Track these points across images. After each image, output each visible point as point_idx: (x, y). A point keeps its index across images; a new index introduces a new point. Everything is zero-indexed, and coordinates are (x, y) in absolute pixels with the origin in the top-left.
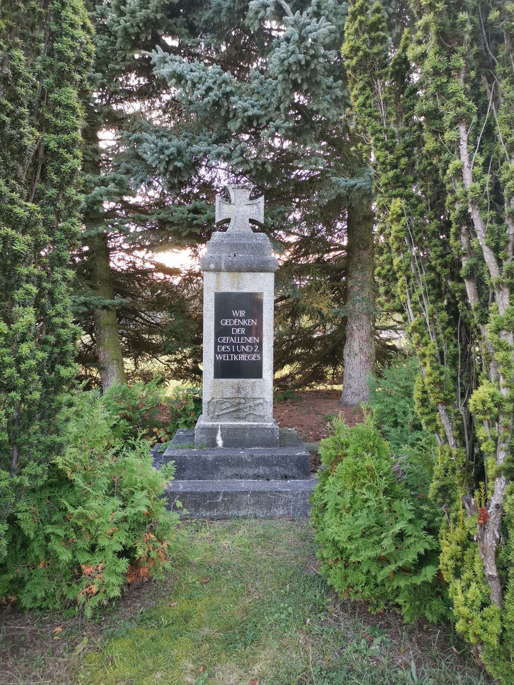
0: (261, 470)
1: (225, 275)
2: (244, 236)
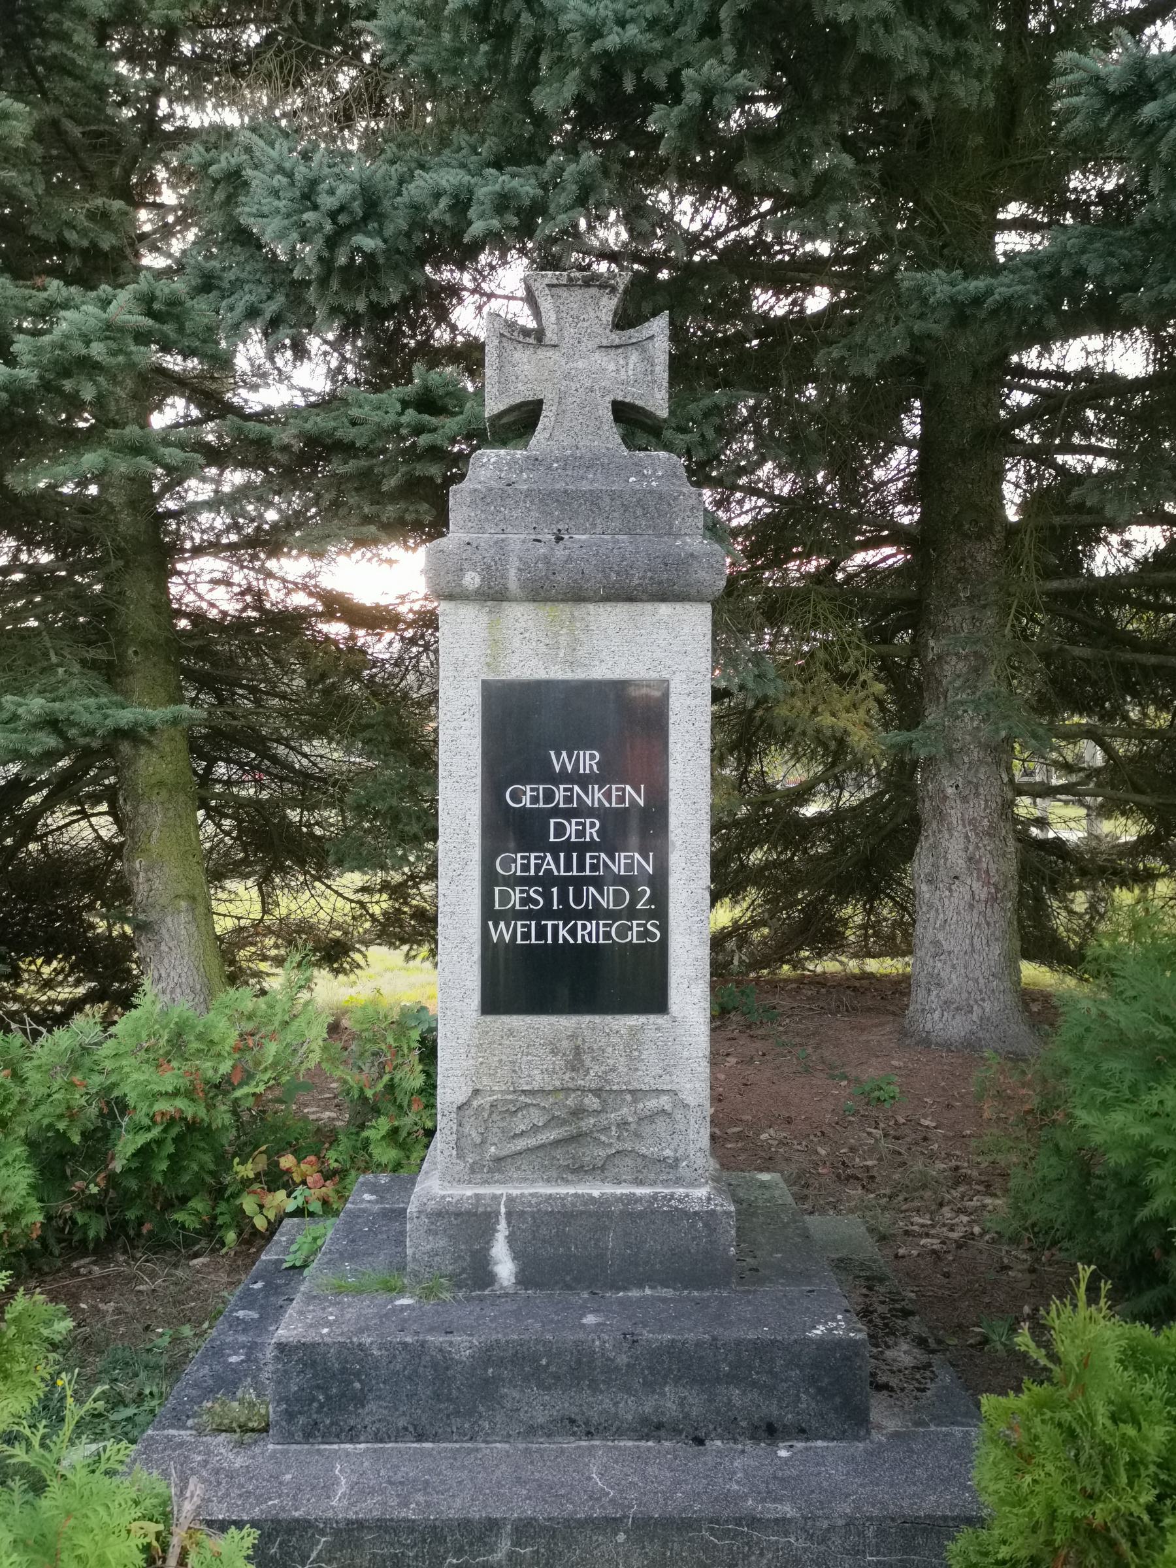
0: (669, 1401)
1: (521, 617)
2: (592, 463)
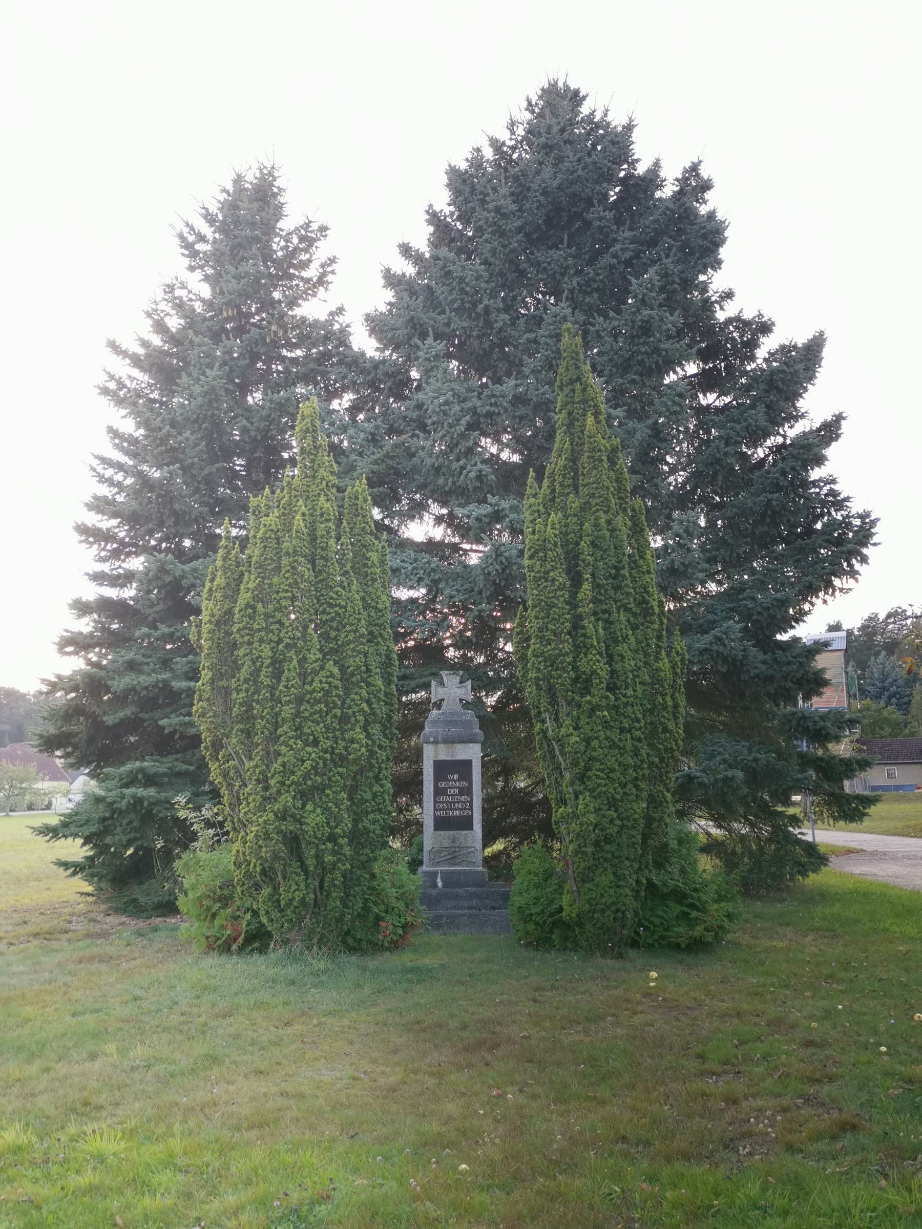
0: (474, 903)
